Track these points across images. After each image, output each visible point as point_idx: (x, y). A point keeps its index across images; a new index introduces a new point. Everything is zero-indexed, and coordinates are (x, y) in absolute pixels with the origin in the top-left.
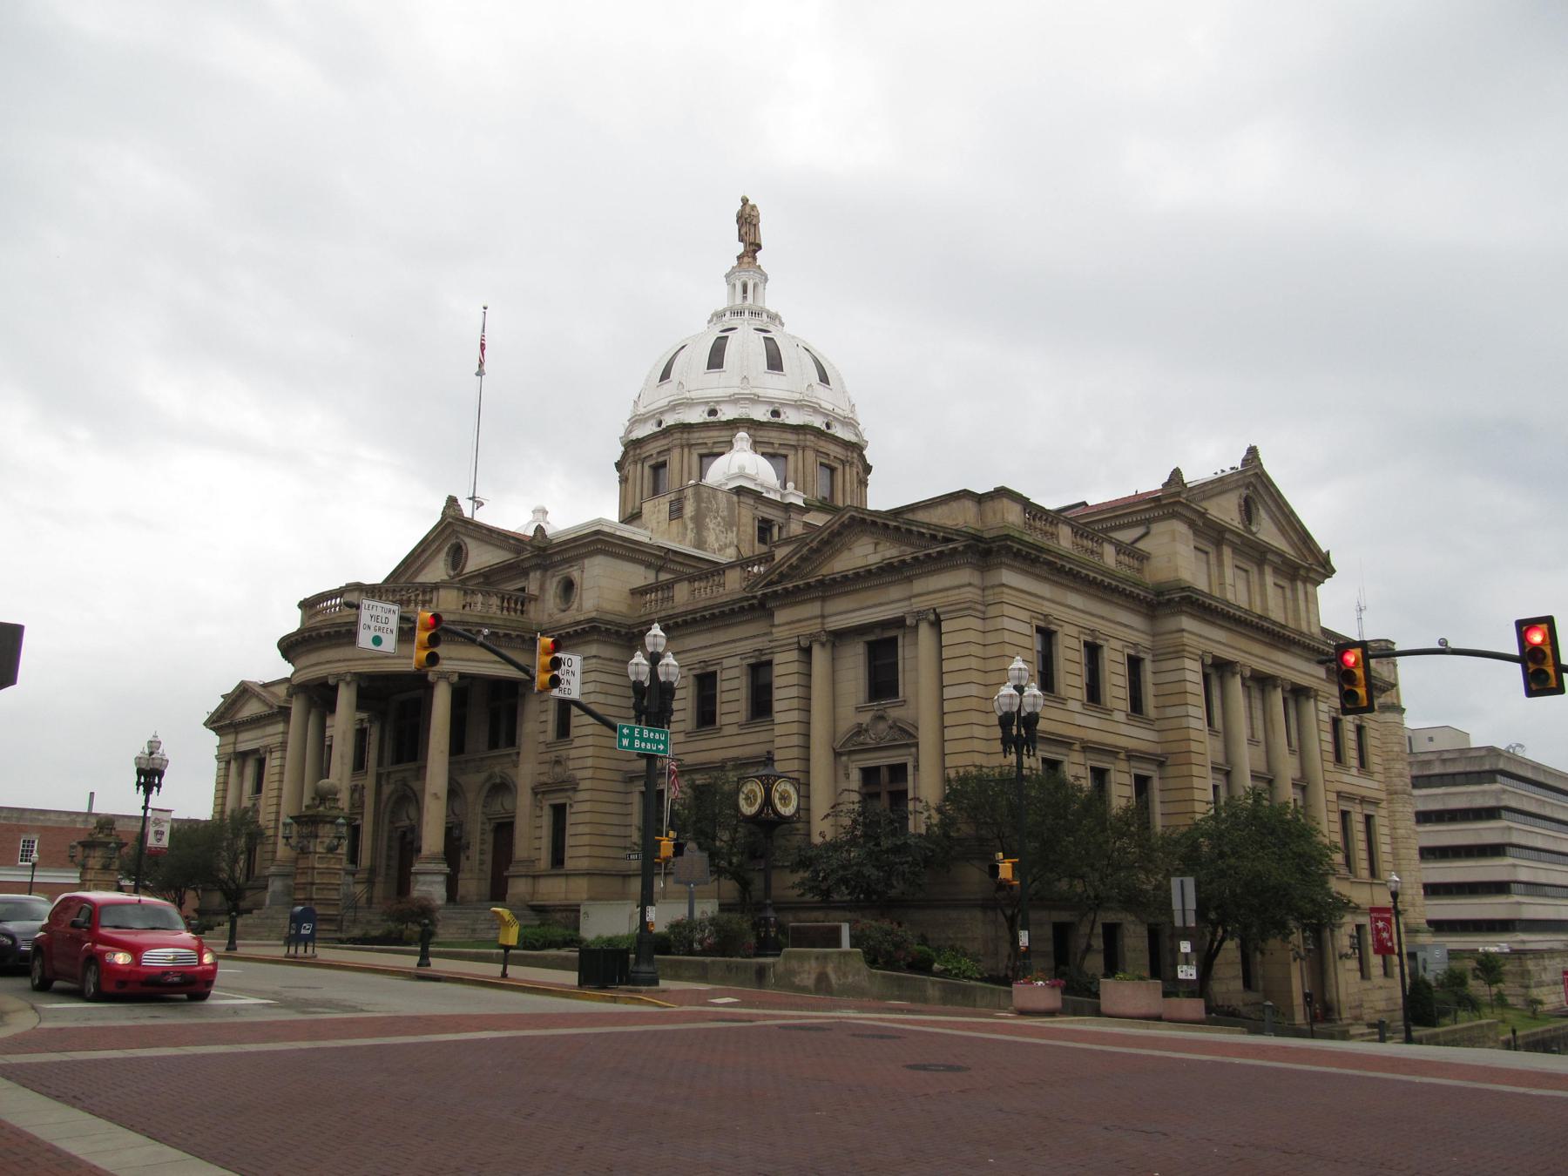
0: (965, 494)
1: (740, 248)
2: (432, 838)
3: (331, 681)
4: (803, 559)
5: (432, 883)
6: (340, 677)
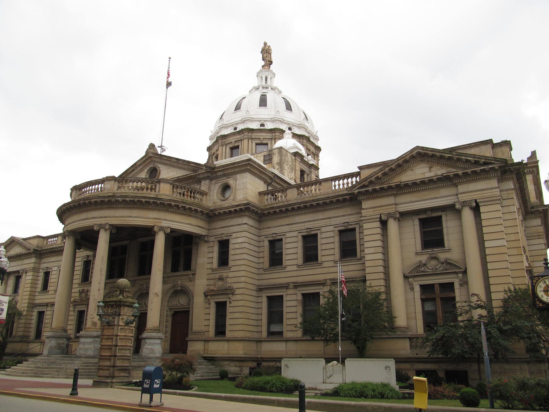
0: (489, 142)
1: (263, 63)
2: (154, 317)
3: (96, 228)
4: (385, 174)
5: (154, 344)
6: (101, 226)
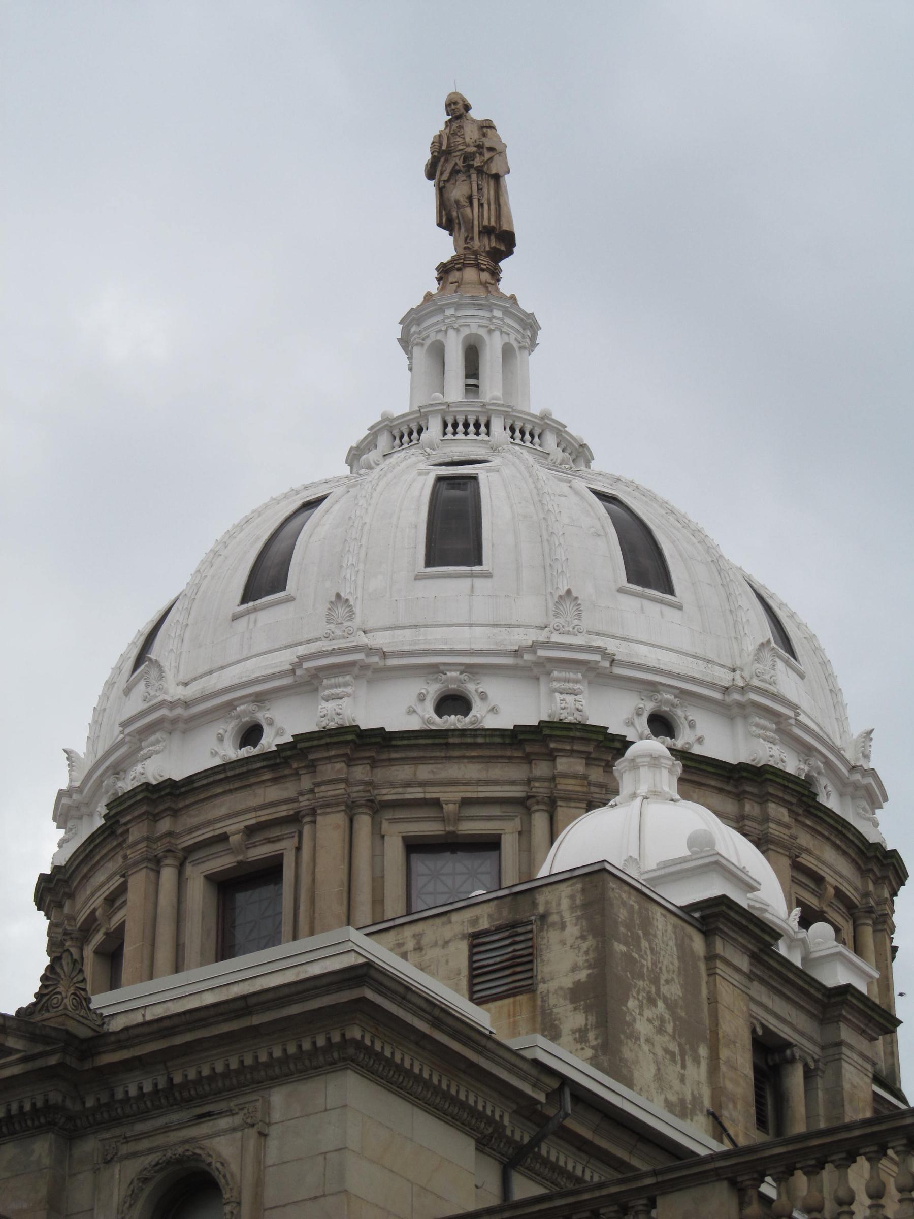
1: (445, 247)
